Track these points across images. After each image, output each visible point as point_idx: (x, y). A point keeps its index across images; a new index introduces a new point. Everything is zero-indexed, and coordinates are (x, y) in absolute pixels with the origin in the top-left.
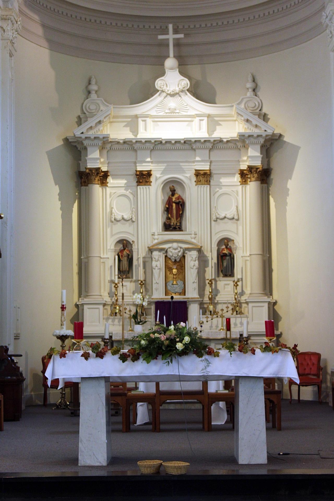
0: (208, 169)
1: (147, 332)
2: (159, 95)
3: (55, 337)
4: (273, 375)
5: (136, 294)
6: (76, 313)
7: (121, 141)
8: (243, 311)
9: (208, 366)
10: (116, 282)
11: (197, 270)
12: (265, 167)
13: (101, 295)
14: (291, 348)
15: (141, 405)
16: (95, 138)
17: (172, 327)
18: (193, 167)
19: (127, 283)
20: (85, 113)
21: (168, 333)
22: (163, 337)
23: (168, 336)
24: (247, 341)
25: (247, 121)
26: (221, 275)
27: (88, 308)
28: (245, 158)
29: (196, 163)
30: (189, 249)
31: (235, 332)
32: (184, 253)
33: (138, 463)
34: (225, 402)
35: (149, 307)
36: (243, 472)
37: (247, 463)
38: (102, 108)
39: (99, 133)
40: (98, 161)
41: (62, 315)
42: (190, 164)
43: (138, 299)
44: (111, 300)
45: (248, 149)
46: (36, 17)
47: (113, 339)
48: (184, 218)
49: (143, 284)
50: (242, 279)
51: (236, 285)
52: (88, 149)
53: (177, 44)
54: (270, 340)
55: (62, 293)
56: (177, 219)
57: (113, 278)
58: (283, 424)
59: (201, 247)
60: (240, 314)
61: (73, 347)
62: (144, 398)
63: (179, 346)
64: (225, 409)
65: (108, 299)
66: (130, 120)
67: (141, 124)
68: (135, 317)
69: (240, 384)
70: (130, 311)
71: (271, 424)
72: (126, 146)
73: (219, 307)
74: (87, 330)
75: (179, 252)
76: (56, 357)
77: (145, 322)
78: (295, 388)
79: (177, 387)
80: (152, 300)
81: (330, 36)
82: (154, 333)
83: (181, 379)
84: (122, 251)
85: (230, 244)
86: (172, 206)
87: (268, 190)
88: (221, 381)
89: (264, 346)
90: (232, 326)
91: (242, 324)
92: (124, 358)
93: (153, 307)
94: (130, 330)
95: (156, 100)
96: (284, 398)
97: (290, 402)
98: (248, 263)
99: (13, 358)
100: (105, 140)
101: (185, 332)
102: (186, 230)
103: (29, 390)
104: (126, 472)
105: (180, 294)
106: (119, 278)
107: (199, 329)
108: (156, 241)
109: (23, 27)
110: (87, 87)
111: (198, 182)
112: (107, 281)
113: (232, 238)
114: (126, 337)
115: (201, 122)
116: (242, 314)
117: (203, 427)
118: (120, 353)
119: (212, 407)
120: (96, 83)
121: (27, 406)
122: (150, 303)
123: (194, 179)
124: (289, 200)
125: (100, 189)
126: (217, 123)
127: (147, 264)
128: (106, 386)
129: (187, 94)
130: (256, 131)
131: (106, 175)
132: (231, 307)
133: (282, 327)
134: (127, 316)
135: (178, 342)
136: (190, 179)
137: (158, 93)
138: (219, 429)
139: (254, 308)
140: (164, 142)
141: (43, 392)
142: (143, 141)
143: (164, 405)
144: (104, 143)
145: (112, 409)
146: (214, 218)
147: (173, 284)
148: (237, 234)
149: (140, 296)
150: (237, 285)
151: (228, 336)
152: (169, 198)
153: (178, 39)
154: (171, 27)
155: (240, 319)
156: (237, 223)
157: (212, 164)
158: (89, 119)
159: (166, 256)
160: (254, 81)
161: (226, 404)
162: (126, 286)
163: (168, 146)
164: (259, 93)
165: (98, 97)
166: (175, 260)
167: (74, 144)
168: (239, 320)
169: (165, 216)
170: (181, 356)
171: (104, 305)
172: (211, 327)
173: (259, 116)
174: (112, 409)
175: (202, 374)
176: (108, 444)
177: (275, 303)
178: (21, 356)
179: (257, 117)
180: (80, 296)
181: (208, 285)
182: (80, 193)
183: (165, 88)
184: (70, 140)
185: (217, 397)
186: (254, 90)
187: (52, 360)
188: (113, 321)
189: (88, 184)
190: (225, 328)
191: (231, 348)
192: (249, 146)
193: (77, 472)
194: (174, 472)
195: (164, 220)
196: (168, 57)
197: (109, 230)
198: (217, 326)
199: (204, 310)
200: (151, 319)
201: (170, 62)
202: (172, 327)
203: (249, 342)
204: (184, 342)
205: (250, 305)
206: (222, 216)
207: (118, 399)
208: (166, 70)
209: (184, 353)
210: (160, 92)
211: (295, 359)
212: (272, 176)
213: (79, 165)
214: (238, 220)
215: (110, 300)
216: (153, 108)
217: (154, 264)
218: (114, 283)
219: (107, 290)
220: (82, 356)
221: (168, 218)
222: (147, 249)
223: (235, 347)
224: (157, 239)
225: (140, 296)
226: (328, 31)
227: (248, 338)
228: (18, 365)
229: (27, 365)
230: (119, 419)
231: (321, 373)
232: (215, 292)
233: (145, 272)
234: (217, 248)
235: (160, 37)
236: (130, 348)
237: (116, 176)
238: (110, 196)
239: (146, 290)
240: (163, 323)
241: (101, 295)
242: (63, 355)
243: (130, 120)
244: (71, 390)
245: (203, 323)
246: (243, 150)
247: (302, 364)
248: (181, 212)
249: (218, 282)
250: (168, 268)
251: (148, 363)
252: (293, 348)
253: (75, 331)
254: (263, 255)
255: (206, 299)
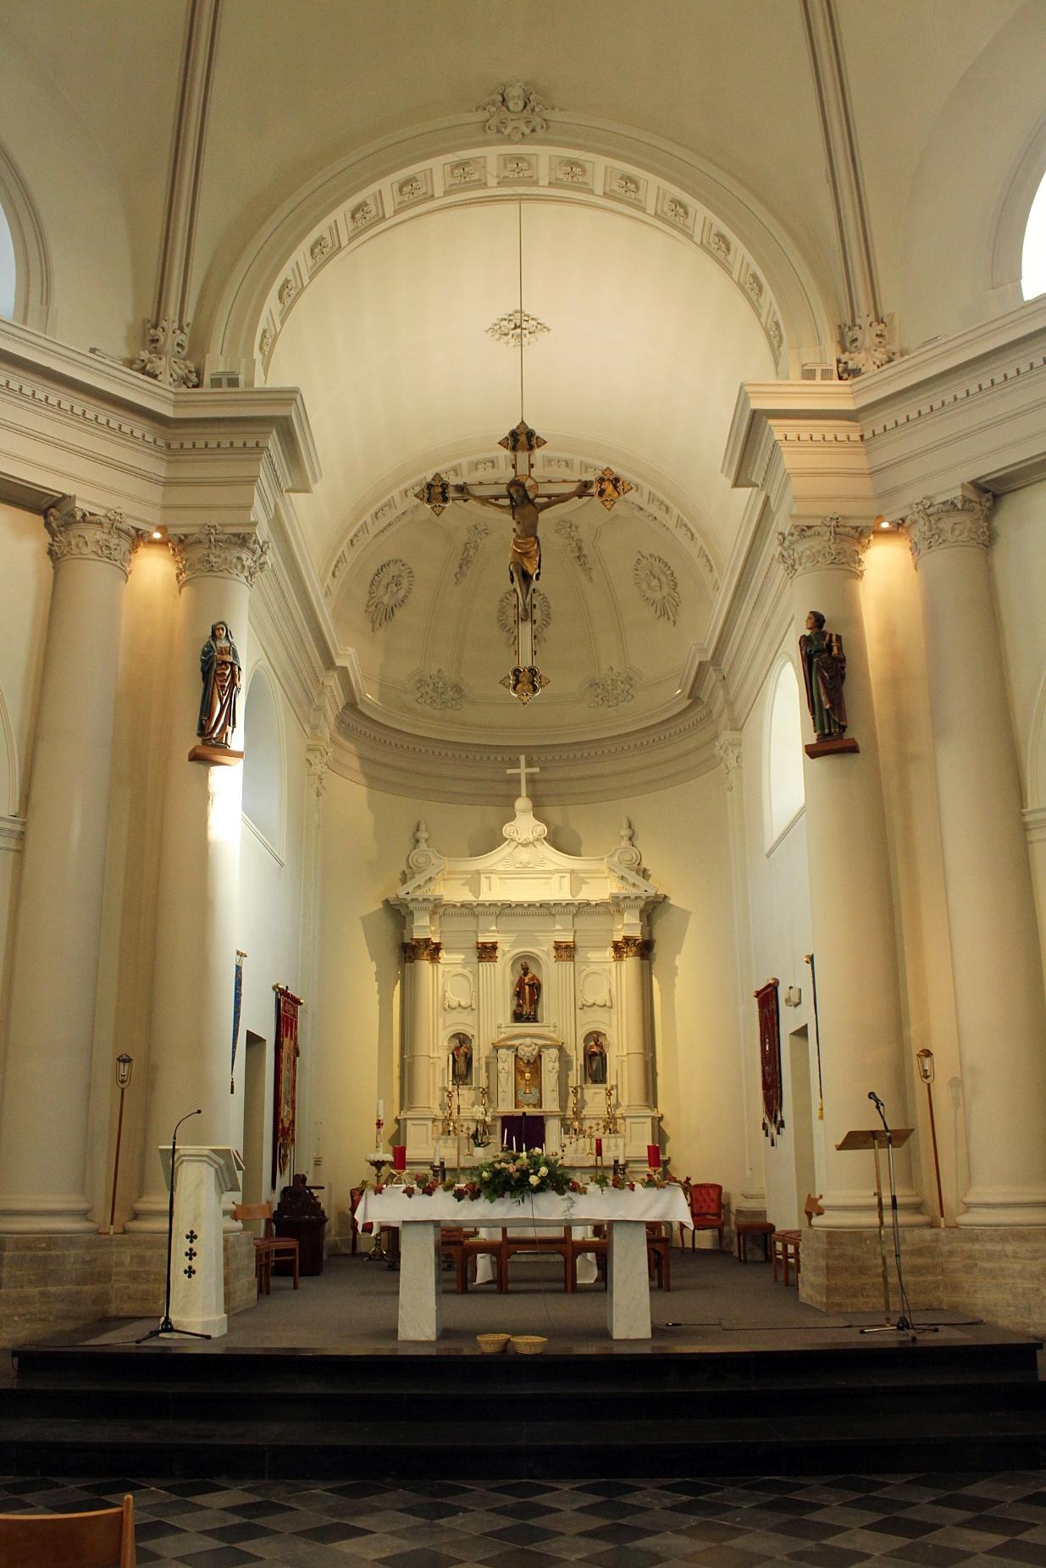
0: (572, 940)
1: (491, 1160)
2: (508, 844)
3: (368, 1163)
4: (659, 1217)
5: (476, 1107)
6: (396, 1132)
7: (458, 904)
8: (618, 1129)
9: (572, 1206)
10: (450, 1090)
11: (557, 1075)
12: (647, 938)
13: (429, 1108)
14: (683, 1182)
15: (482, 1257)
16: (424, 900)
17: (524, 1154)
18: (551, 938)
19: (464, 1091)
20: (411, 868)
21: (519, 1162)
22: (512, 1168)
23: (519, 1167)
24: (624, 1169)
25: (622, 878)
26: (589, 1080)
27: (414, 1125)
28: (620, 927)
29: (555, 933)
30: (546, 1047)
31: (608, 1158)
32: (540, 1051)
33: (478, 1338)
34: (594, 1254)
35: (494, 1123)
36: (619, 1350)
37: (624, 1338)
38: (434, 860)
39: (429, 893)
40: (428, 930)
41: (379, 1133)
42: (548, 934)
43: (478, 1112)
44: (443, 1113)
45: (623, 914)
46: (352, 747)
47: (446, 1166)
48: (539, 1006)
49: (485, 1092)
50: (617, 1086)
51: (609, 1094)
52: (415, 914)
53: (531, 780)
54: (655, 1171)
55: (378, 1104)
56: (530, 1005)
57: (446, 1085)
58: (673, 1283)
59: (563, 1043)
60: (614, 1133)
61: (391, 1179)
62: (487, 1248)
63: (534, 1180)
64: (595, 1262)
65: (439, 1113)
66: (470, 876)
67: (484, 882)
68: (475, 1136)
69: (614, 1231)
70: (468, 1129)
71: (656, 1283)
72: (464, 910)
73: (587, 1124)
74: (410, 1154)
75: (533, 1050)
76: (370, 1193)
77: (489, 1144)
78: (687, 1234)
79: (530, 1233)
80: (497, 1115)
81: (726, 771)
82: (499, 1162)
83: (536, 1223)
84: (457, 1049)
85: (601, 1039)
86: (524, 989)
87: (651, 968)
88: (589, 1227)
89: (646, 1180)
90: (604, 1149)
91: (617, 1146)
92: (459, 1195)
93: (499, 1124)
94: (468, 1155)
95: (504, 851)
96: (674, 1245)
97: (682, 1252)
98: (625, 1064)
99: (312, 1190)
100: (437, 902)
101: (541, 1160)
102: (542, 1021)
103: (333, 1233)
104: (462, 1349)
105: (535, 1106)
106: (453, 1084)
107: (560, 1153)
108: (503, 1036)
109: (334, 759)
110: (414, 835)
111: (558, 958)
112: (438, 1089)
113: (603, 1032)
114: (462, 1165)
115: (563, 879)
116: (618, 1132)
117: (566, 1287)
118: (454, 1189)
119: (577, 1260)
120: (427, 829)
121: (329, 1256)
122: (494, 1118)
123: (553, 953)
124: (677, 980)
125: (430, 966)
126: (583, 881)
127: (491, 1066)
128: (435, 1234)
129: (543, 844)
130: (634, 892)
131: (437, 948)
132: (602, 1124)
133: (671, 1151)
134: (464, 1135)
135: (532, 1174)
136: (548, 954)
137: (506, 843)
138: (586, 1290)
139: (633, 1125)
140: (513, 905)
141: (351, 1237)
142: (487, 904)
143: (512, 1256)
144: (436, 906)
145: (443, 1262)
146: (579, 1004)
147: (525, 1093)
148: (610, 1026)
149: (482, 1109)
150: (611, 1094)
151: (599, 1163)
152: (521, 978)
153: (532, 774)
154: (523, 758)
155: (614, 1140)
156: (610, 1012)
157: (577, 934)
158: (416, 876)
159: (516, 1056)
160: (630, 827)
161: (597, 1255)
162: (462, 1095)
163: (519, 910)
164: (636, 843)
165: (429, 846)
166: (529, 1061)
167: (398, 908)
168: (613, 1141)
169: (515, 1002)
170: (535, 1193)
171: (434, 1120)
172: (576, 1150)
173: (637, 872)
174: (443, 1262)
175: (563, 1218)
176: (438, 1311)
177: (661, 1119)
178: (323, 1188)
179: (634, 873)
180: (401, 1108)
181: (572, 1094)
182: (403, 972)
183: (515, 836)
184: (392, 903)
185: (584, 1247)
186: (630, 839)
187: (364, 1197)
188: (445, 1143)
189: (415, 959)
190: (594, 1152)
191: (602, 1182)
192: (624, 911)
193: (397, 1350)
194: (526, 1351)
195: (514, 1007)
196: (519, 796)
197: (440, 1021)
198: (584, 1150)
199: (566, 1128)
200: (496, 1140)
201: (522, 803)
202: (524, 1154)
203: (627, 1170)
204: (539, 1175)
205: (628, 1120)
206: (591, 1002)
207: (451, 1249)
208: (517, 813)
209: (539, 1189)
210: (508, 841)
211: (688, 1197)
212: (655, 950)
213: (402, 935)
214: (611, 1007)
215: (441, 1114)
216: (498, 862)
217: (500, 1065)
218: (447, 1091)
219: (438, 1102)
220: (404, 1192)
221: (519, 1005)
222: (491, 1047)
223: (608, 1180)
224: (505, 1033)
225: (482, 1109)
226: (722, 766)
227: (625, 1166)
228: (318, 1200)
229: (330, 1200)
230: (453, 1275)
231: (722, 1211)
232: (581, 1104)
233: (488, 1077)
234: (583, 1045)
235: (509, 771)
236: (468, 1182)
237: (450, 950)
238: (443, 976)
239: (490, 1101)
240: (513, 1149)
241: (429, 1108)
242: (378, 1191)
243: (470, 876)
244: (389, 1233)
245: (565, 1146)
246: (617, 916)
247: (697, 1200)
248: (536, 997)
249: (586, 1091)
250: (519, 1072)
251: (491, 1202)
252: (685, 1182)
253: (395, 1156)
254: (644, 1054)
255: (570, 1114)
